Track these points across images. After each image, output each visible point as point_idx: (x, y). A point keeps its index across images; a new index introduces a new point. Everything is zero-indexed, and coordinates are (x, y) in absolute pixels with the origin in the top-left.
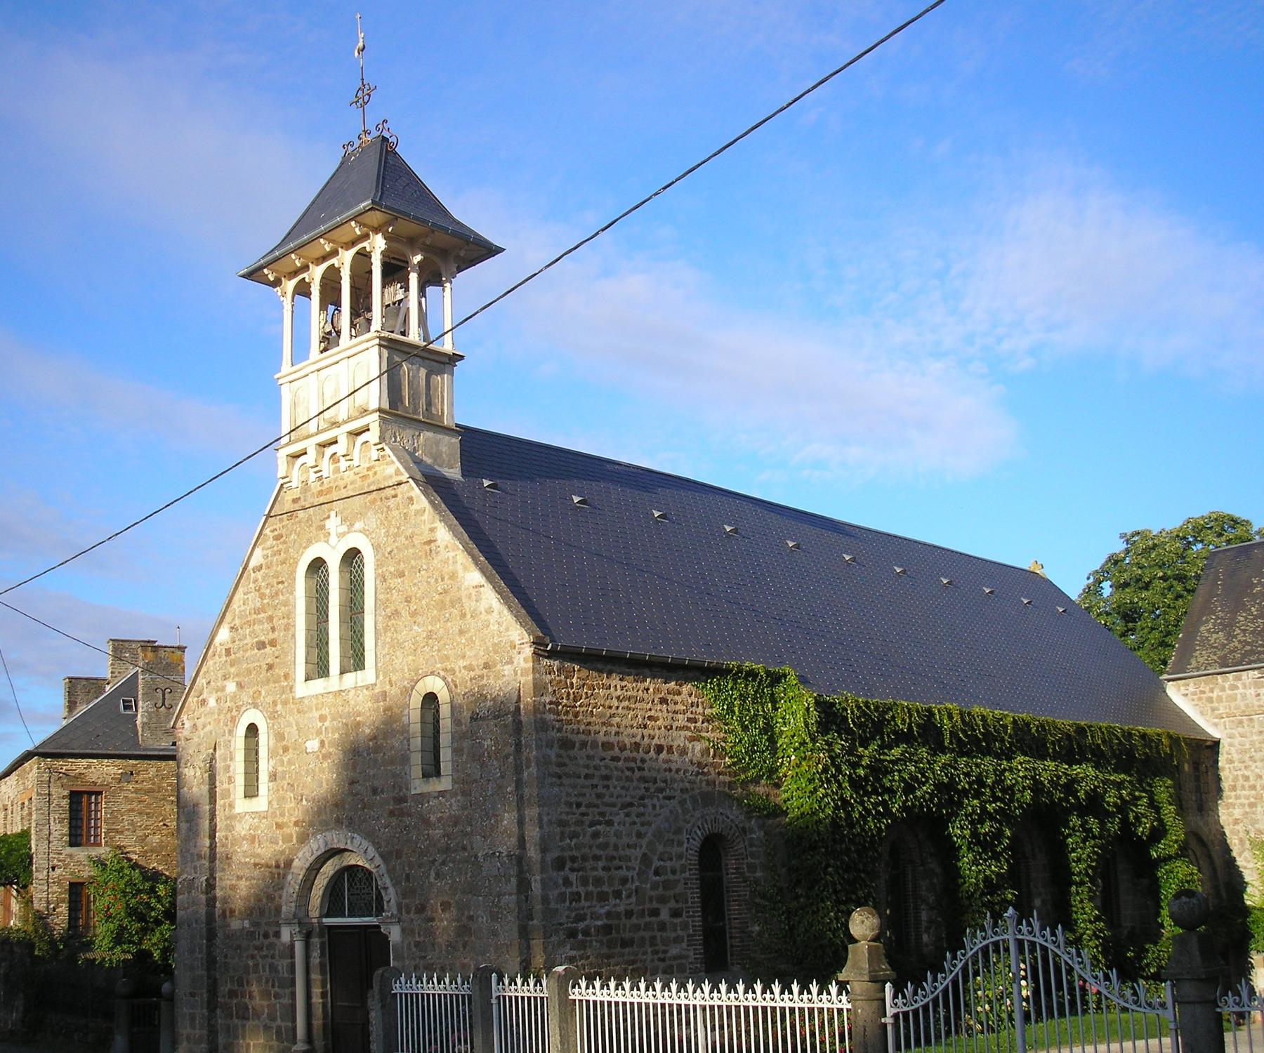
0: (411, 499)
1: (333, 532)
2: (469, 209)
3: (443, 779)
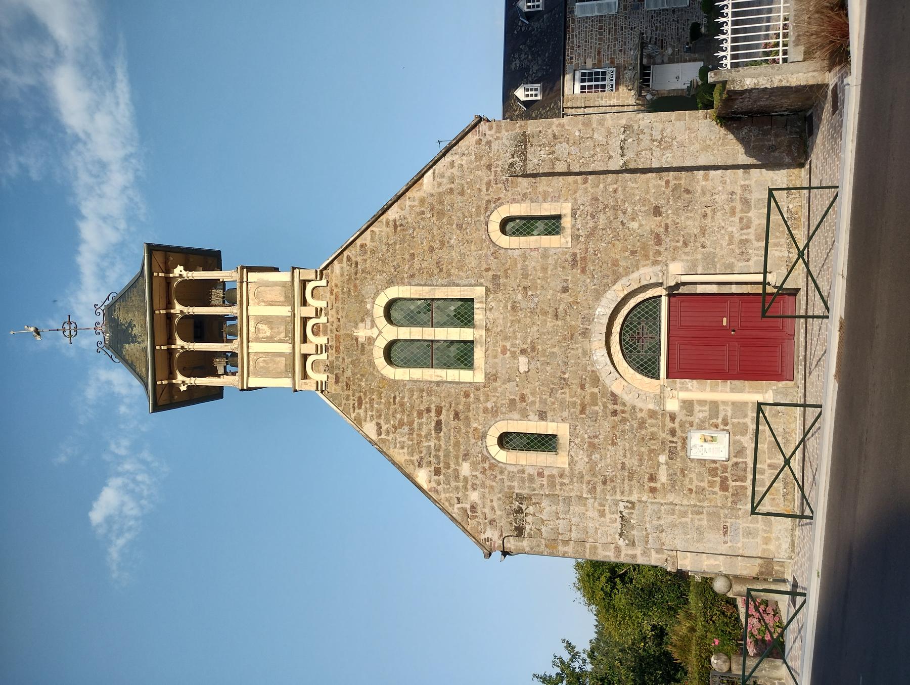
0: (362, 246)
3: (559, 434)
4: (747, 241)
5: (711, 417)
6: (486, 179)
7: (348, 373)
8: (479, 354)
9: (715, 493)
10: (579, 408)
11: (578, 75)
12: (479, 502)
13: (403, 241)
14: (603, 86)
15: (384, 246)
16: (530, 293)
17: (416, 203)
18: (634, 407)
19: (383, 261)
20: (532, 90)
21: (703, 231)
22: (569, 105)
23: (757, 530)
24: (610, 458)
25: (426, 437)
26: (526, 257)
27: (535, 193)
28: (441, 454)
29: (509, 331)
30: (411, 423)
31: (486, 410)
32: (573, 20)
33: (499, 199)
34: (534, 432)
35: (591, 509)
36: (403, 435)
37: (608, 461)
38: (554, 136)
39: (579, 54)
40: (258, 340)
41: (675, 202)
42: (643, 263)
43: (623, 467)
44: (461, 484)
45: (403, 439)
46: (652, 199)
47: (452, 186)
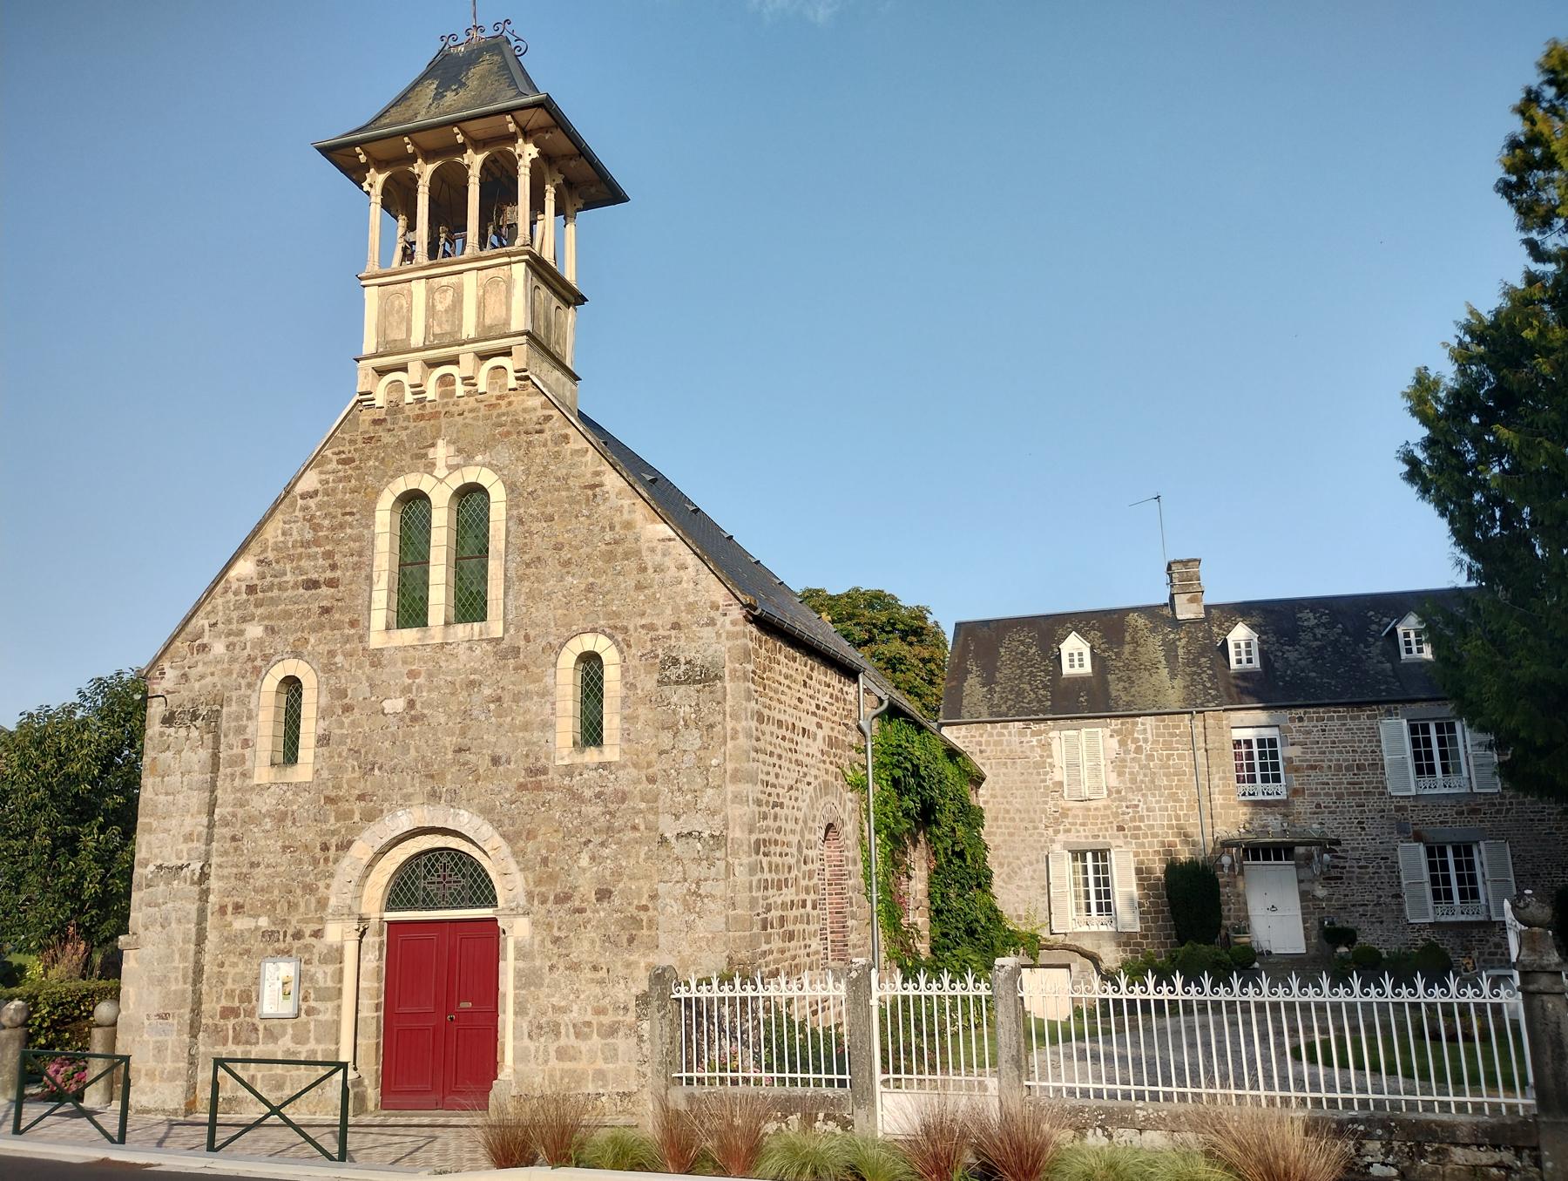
0: (566, 437)
1: (441, 463)
3: (299, 767)
4: (558, 1034)
6: (658, 622)
7: (387, 438)
8: (410, 636)
9: (219, 999)
10: (333, 794)
11: (1267, 733)
12: (211, 656)
13: (573, 501)
14: (1252, 779)
15: (564, 471)
16: (492, 706)
17: (626, 516)
18: (332, 876)
19: (543, 474)
20: (1248, 653)
22: (1210, 722)
23: (164, 1061)
24: (265, 843)
25: (298, 567)
26: (543, 696)
27: (635, 703)
28: (275, 593)
29: (440, 680)
30: (317, 542)
31: (332, 654)
32: (1375, 717)
33: (629, 646)
34: (302, 730)
35: (194, 821)
37: (262, 843)
38: (711, 726)
39: (1309, 733)
40: (430, 292)
41: (617, 921)
42: (530, 877)
43: (253, 865)
44: (234, 626)
45: (295, 532)
46: (621, 885)
47: (650, 571)
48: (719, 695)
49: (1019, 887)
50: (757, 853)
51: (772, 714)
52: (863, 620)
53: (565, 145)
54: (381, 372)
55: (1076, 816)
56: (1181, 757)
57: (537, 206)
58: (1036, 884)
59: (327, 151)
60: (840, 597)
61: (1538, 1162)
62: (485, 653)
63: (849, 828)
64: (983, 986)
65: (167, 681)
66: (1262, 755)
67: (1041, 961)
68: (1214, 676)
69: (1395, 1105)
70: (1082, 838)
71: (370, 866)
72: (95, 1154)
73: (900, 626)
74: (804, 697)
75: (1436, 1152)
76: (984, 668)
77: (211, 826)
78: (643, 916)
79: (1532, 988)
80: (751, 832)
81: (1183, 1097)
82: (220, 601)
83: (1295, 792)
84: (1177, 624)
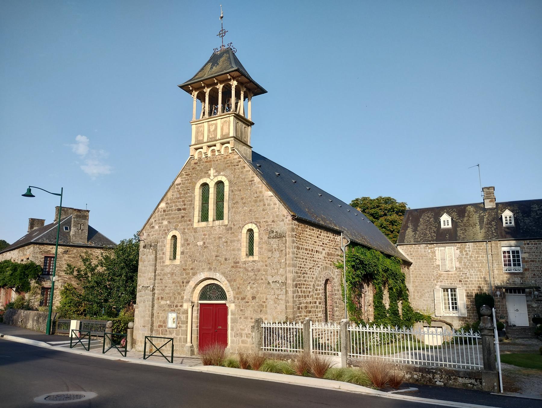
0: (244, 167)
1: (212, 175)
2: (256, 76)
3: (176, 260)
4: (242, 336)
5: (181, 321)
6: (268, 220)
7: (198, 168)
8: (204, 224)
11: (518, 249)
13: (246, 185)
14: (510, 265)
17: (260, 189)
21: (246, 318)
22: (493, 245)
28: (170, 212)
29: (212, 237)
30: (180, 198)
31: (184, 229)
36: (176, 195)
38: (282, 251)
40: (209, 126)
43: (166, 287)
44: (160, 221)
48: (284, 242)
49: (424, 300)
50: (296, 287)
51: (303, 247)
52: (382, 208)
53: (245, 80)
54: (196, 149)
55: (444, 277)
56: (482, 257)
57: (238, 97)
58: (430, 299)
59: (181, 87)
60: (374, 200)
61: (481, 383)
62: (223, 229)
63: (336, 280)
64: (393, 330)
65: (144, 237)
66: (514, 257)
67: (432, 325)
68: (497, 228)
69: (441, 365)
70: (447, 284)
71: (195, 288)
72: (117, 358)
73: (396, 209)
74: (317, 241)
75: (454, 379)
76: (414, 226)
77: (155, 276)
78: (264, 304)
79: (482, 333)
80: (293, 281)
81: (353, 356)
82: (157, 214)
83: (525, 270)
84: (485, 210)
